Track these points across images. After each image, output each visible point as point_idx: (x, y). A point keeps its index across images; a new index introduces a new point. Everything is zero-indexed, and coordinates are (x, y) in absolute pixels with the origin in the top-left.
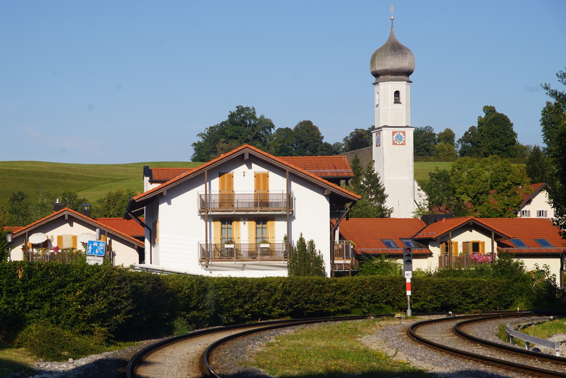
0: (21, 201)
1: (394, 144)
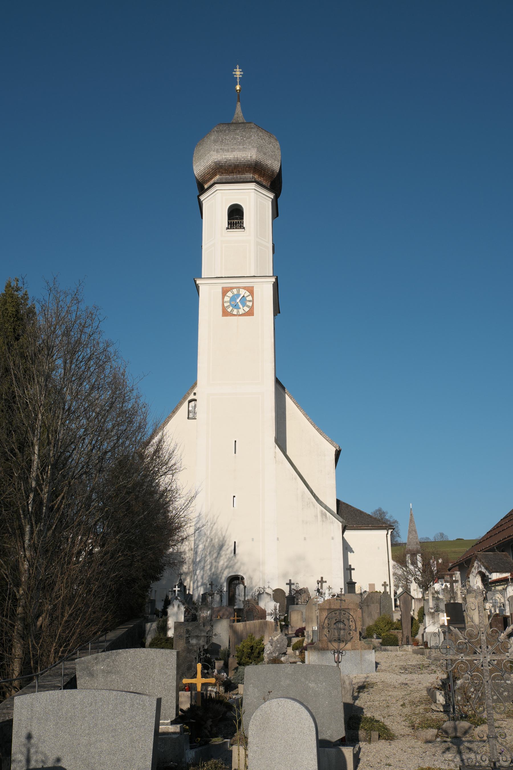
1: (225, 313)
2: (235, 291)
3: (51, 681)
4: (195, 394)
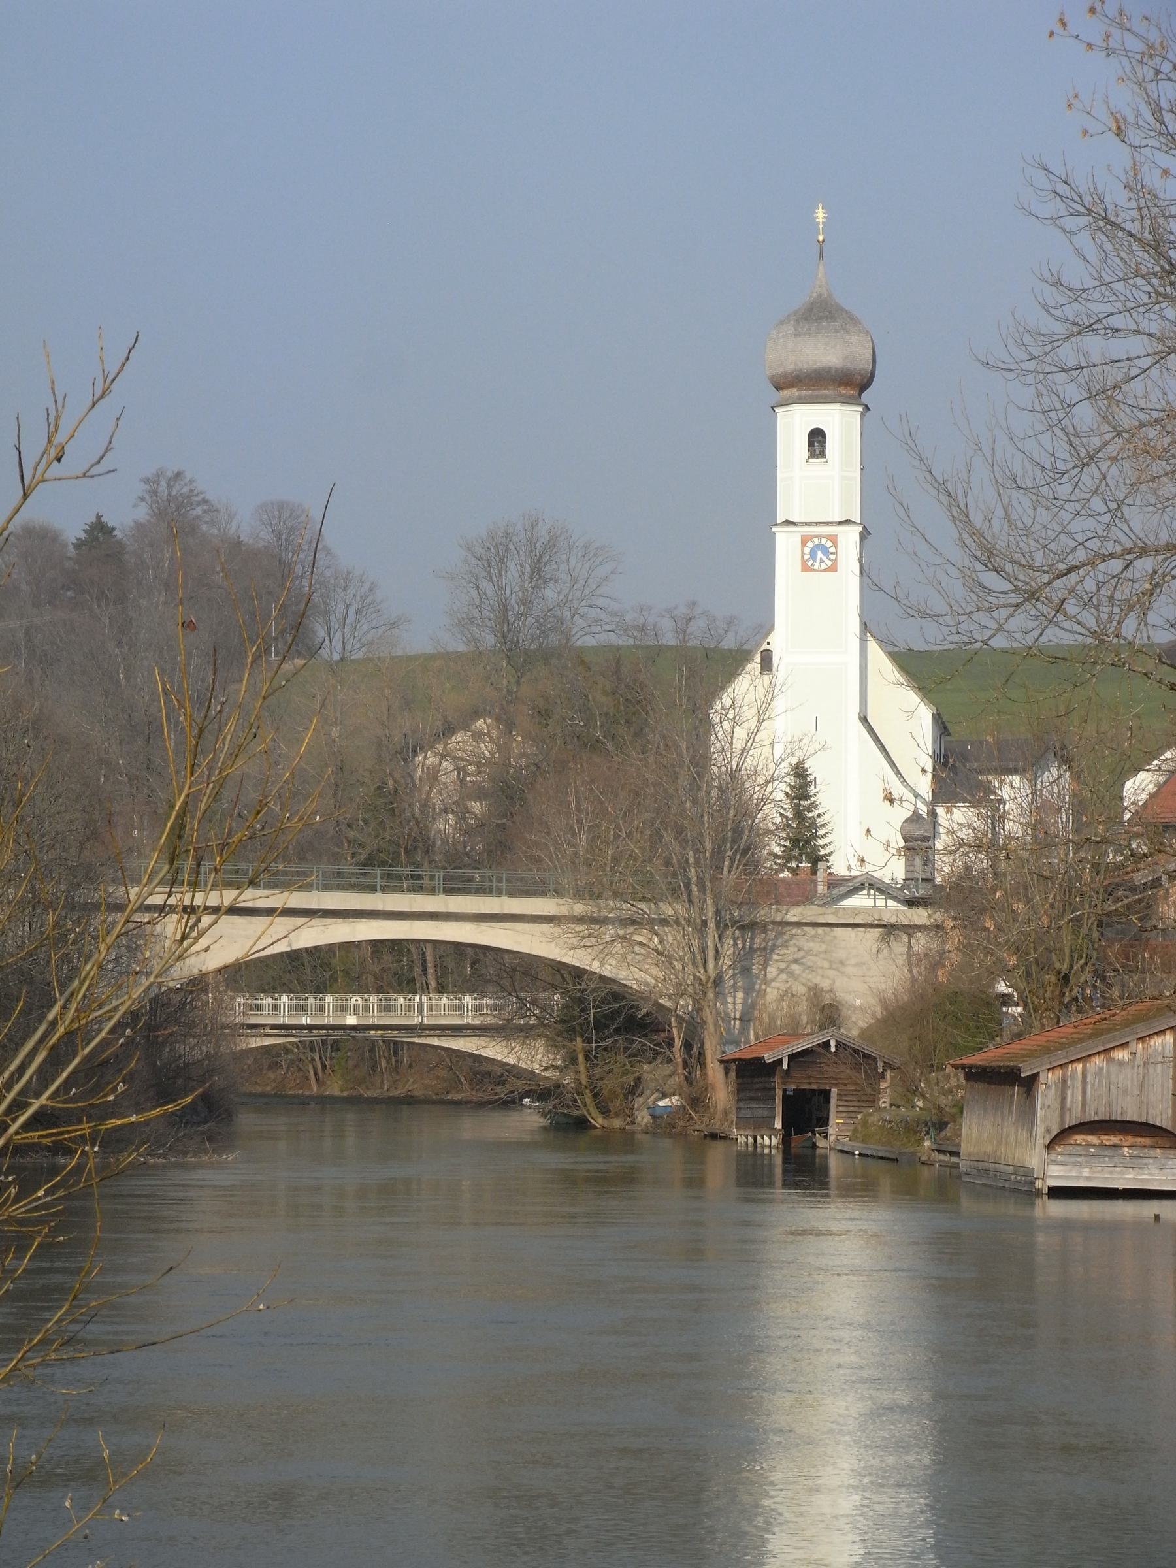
1: (805, 568)
2: (816, 541)
3: (425, 962)
4: (768, 643)
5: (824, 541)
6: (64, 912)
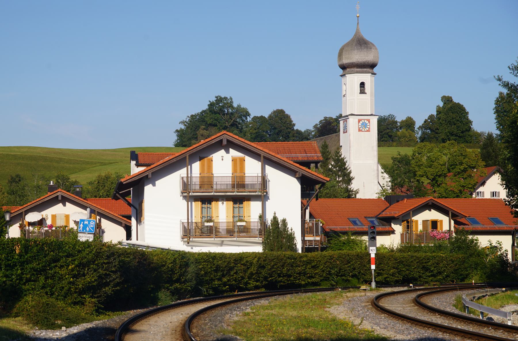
0: (18, 182)
1: (359, 130)
5: (366, 121)
6: (206, 319)
